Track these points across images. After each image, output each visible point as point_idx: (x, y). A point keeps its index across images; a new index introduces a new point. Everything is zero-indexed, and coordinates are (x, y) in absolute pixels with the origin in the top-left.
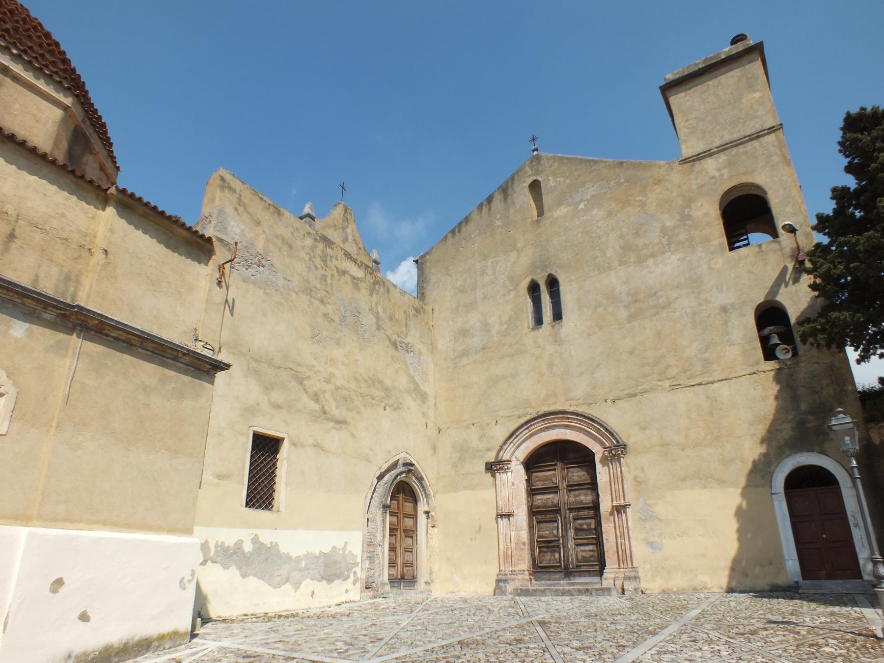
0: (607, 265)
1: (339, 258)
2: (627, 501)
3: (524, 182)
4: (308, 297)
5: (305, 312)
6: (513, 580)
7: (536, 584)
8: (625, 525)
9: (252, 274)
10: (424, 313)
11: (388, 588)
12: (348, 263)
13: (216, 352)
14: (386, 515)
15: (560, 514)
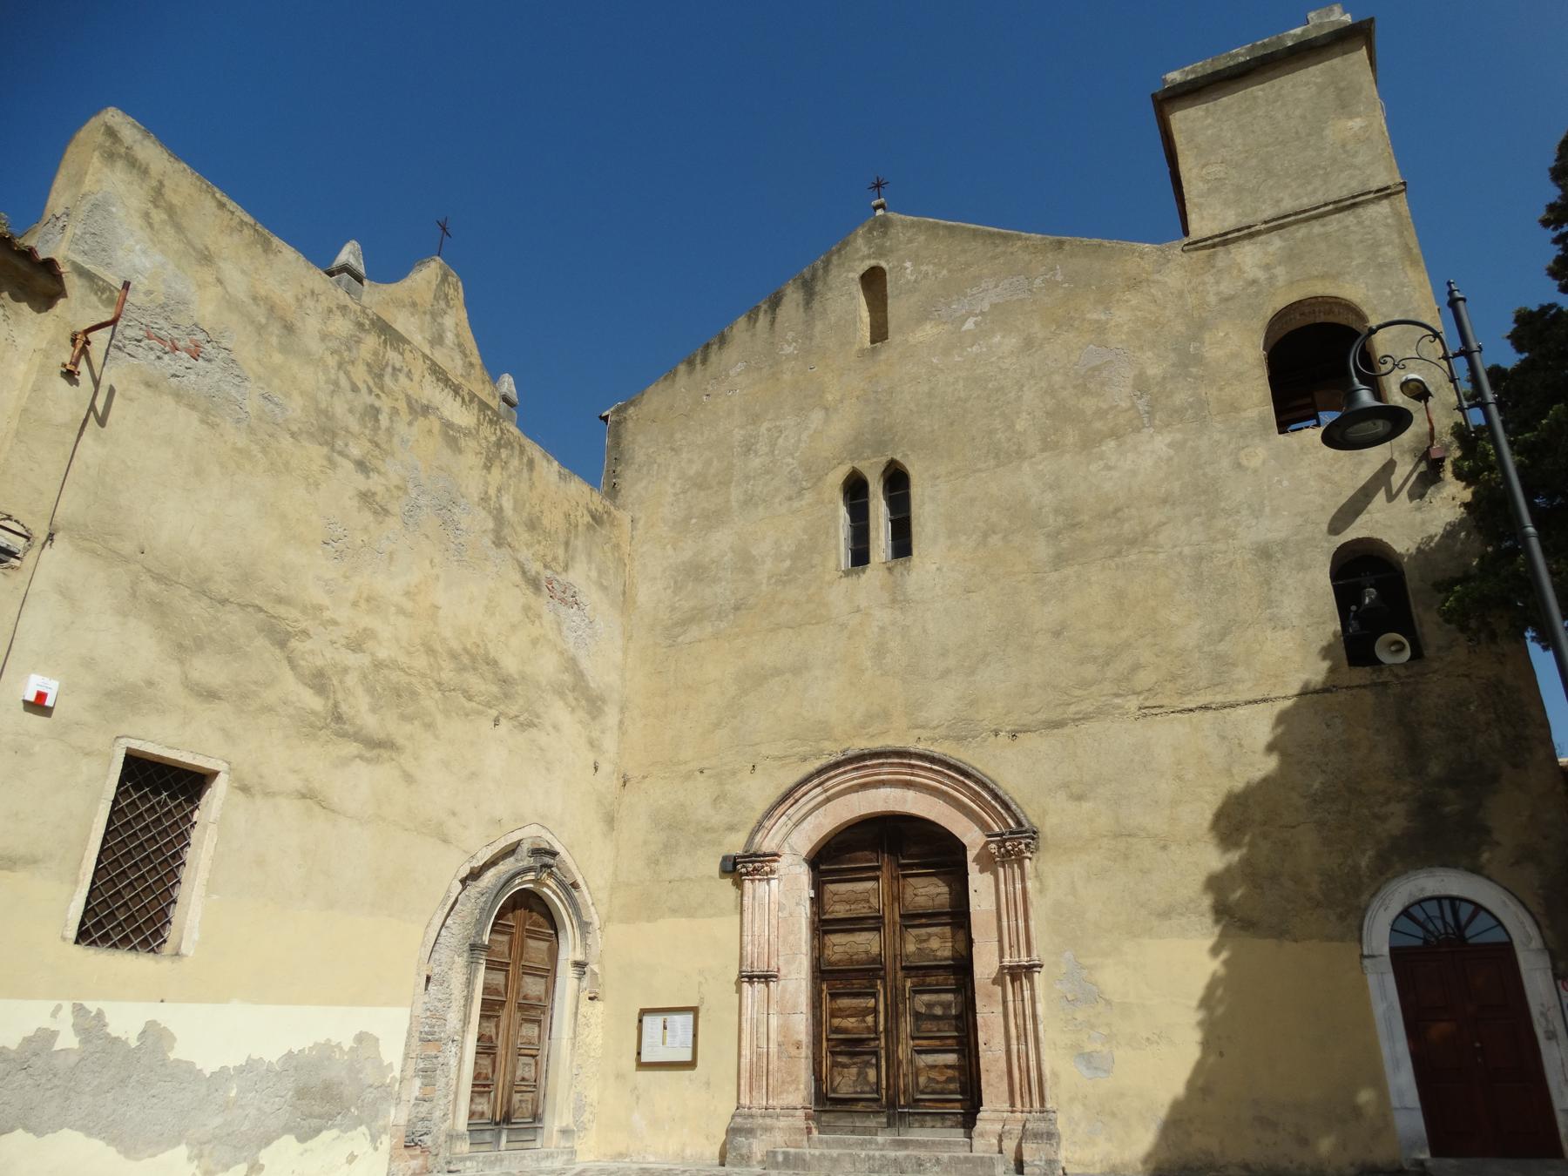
0: (1015, 448)
1: (416, 377)
2: (1034, 956)
3: (852, 270)
4: (325, 450)
5: (311, 480)
6: (768, 1129)
7: (821, 1141)
8: (1028, 1011)
9: (172, 372)
10: (612, 525)
11: (464, 1147)
12: (438, 390)
13: (38, 544)
14: (477, 969)
15: (883, 979)
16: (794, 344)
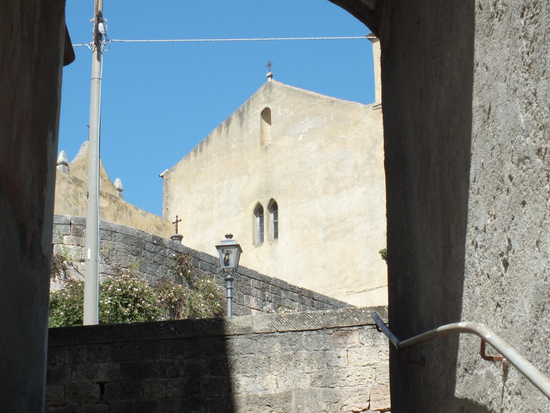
3: (258, 109)
16: (236, 144)
